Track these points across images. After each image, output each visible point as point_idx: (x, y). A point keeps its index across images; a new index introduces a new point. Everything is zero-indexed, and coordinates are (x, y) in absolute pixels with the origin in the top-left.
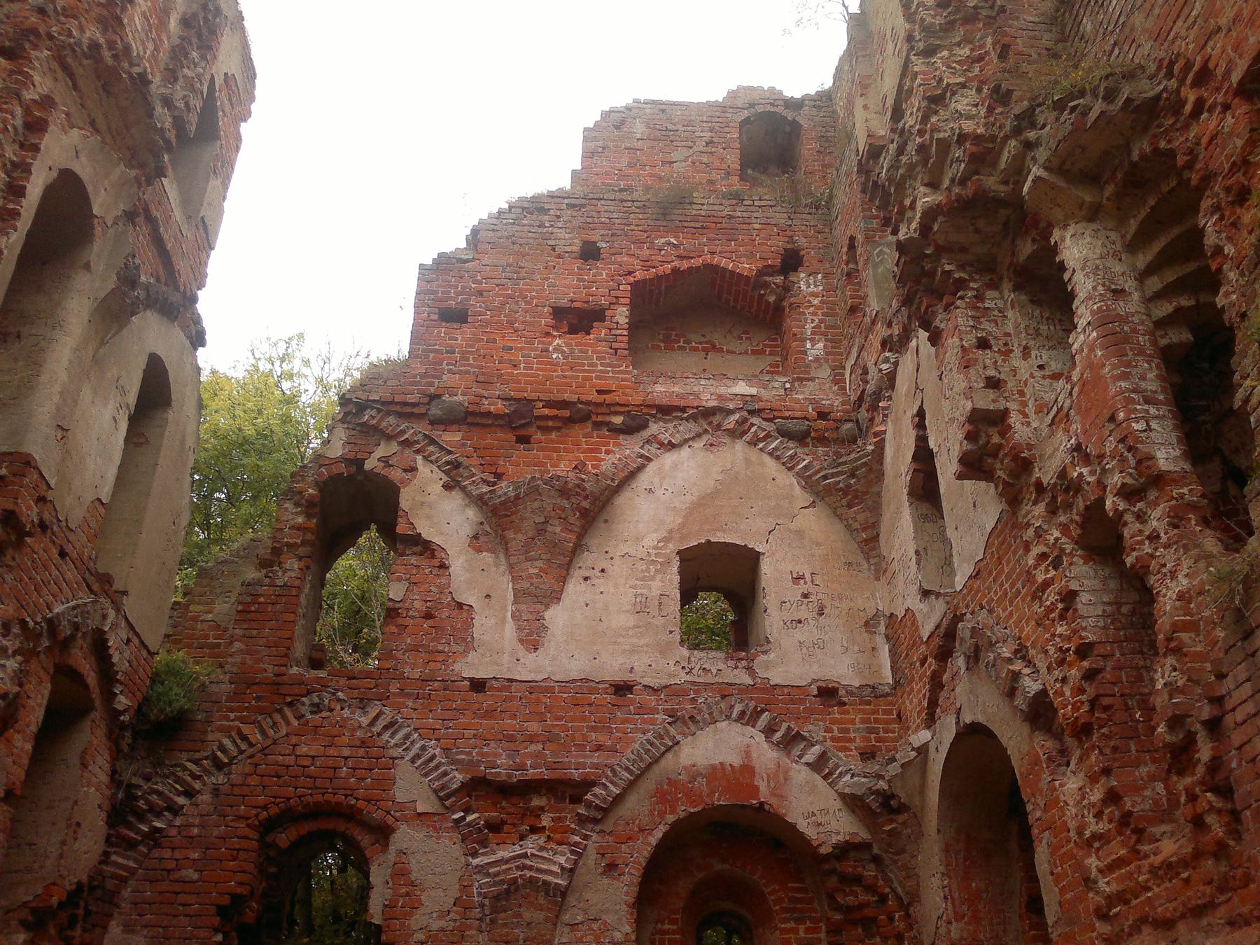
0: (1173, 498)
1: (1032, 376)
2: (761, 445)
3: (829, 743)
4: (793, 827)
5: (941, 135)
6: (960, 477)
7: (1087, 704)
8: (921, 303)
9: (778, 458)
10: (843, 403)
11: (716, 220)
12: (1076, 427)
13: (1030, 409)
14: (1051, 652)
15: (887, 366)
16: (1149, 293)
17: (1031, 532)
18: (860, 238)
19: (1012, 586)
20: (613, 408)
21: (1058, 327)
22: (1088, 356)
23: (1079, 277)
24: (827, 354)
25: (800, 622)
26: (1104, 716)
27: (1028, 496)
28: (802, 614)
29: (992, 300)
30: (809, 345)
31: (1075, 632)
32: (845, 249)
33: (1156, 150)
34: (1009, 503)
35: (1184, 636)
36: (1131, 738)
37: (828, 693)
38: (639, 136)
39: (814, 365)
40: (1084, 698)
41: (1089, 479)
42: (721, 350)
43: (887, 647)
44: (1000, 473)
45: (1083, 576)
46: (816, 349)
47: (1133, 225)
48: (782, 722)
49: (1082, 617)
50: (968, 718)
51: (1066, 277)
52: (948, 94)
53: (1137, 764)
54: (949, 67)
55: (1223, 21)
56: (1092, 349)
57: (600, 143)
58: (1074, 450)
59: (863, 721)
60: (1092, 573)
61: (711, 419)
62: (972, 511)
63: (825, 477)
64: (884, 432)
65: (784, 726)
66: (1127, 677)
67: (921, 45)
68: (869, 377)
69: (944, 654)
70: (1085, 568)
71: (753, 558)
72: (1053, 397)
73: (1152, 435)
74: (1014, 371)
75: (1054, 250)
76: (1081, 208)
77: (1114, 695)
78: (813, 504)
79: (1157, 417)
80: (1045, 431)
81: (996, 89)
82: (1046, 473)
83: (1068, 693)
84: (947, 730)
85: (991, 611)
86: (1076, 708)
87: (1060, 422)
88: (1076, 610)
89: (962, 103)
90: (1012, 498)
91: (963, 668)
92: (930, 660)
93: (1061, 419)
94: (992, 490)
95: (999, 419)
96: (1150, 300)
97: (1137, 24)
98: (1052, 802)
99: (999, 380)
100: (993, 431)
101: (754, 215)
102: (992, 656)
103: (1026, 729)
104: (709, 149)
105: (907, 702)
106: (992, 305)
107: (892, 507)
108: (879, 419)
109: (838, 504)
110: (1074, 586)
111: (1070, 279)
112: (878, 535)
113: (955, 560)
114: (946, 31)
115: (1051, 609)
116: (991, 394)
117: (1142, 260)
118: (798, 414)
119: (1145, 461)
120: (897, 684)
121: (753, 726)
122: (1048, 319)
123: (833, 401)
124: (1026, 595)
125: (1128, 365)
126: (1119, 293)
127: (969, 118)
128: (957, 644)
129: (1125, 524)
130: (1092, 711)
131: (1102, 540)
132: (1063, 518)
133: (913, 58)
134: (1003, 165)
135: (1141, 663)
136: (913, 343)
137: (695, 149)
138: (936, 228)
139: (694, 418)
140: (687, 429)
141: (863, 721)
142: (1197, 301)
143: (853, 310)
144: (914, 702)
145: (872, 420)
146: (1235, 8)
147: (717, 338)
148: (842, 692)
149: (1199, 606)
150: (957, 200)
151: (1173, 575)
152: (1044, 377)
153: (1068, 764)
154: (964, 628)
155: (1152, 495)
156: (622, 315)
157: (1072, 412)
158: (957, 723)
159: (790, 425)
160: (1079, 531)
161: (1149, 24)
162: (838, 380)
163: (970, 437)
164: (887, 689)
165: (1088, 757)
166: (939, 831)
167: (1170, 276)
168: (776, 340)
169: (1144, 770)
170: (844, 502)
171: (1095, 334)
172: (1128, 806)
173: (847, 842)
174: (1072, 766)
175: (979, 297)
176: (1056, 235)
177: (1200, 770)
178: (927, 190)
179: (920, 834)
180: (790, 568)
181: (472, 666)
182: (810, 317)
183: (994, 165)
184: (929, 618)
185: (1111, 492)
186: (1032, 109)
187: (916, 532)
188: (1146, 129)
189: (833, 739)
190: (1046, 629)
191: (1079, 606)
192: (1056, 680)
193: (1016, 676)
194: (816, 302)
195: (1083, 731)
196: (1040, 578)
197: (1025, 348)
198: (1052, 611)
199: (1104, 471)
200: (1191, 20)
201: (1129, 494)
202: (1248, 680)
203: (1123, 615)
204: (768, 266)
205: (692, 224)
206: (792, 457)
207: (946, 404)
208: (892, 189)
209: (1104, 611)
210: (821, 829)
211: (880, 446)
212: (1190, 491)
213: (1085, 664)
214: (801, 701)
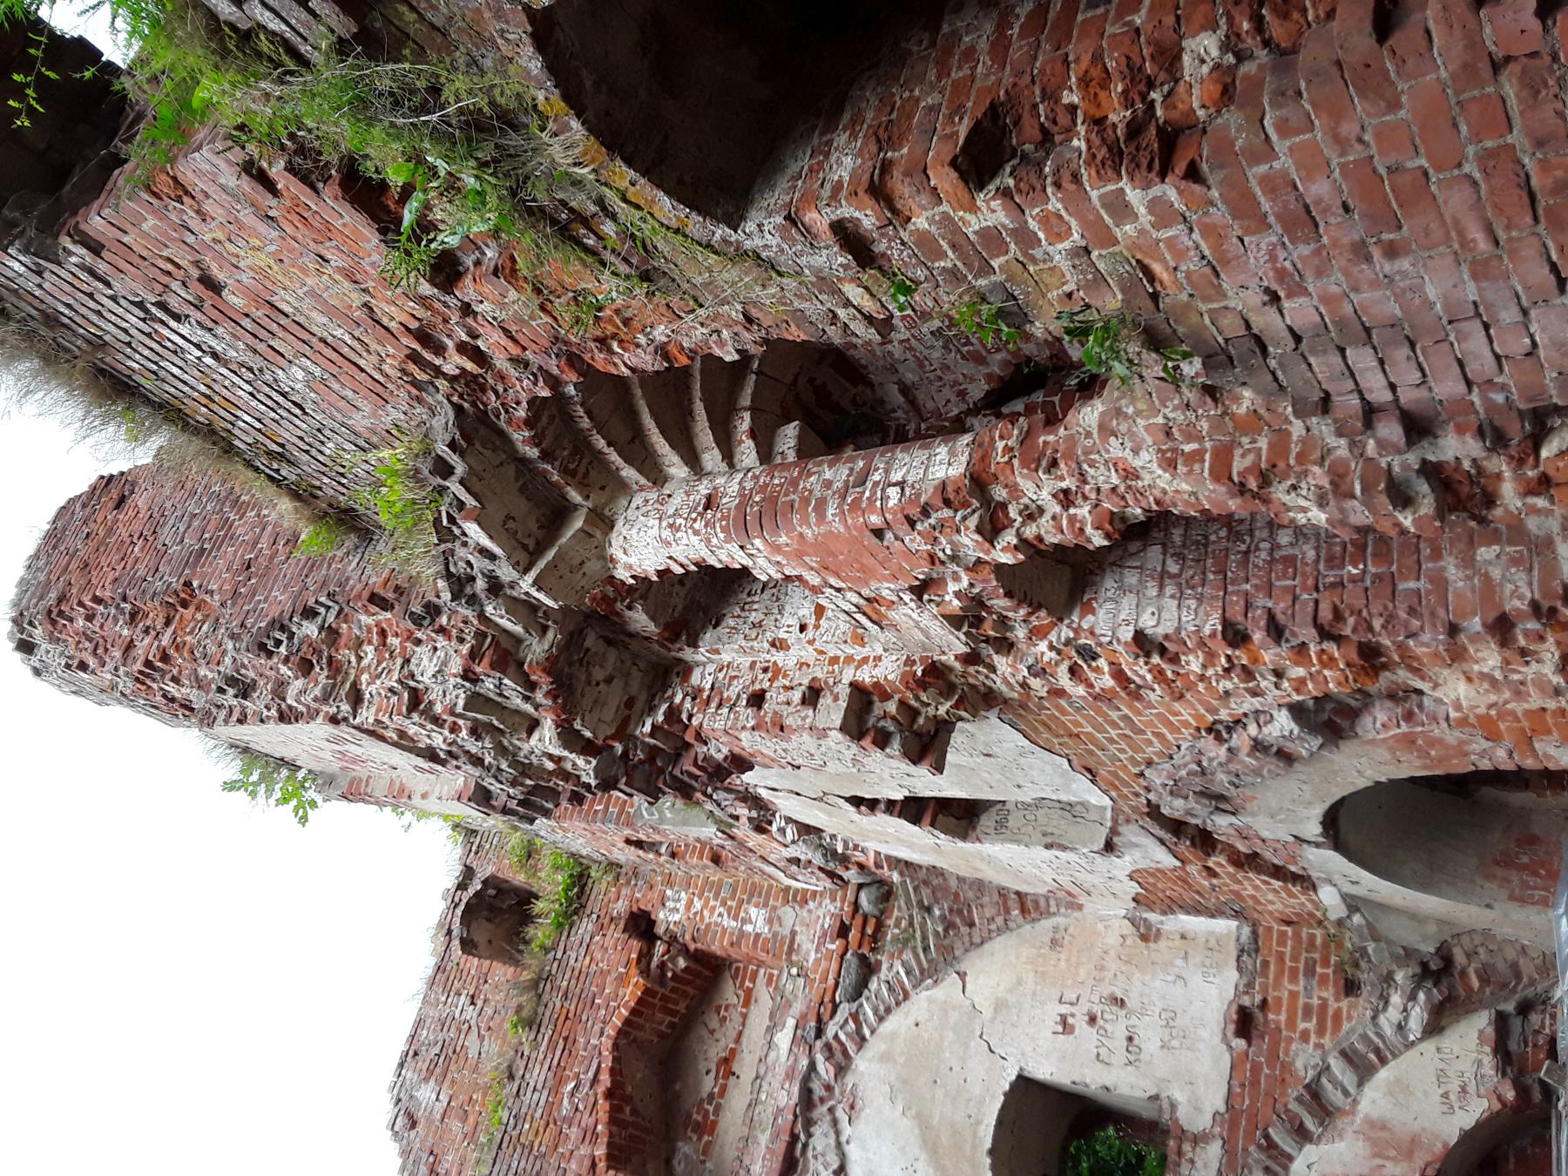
0: (1009, 462)
1: (811, 642)
2: (866, 1032)
3: (1327, 1041)
4: (1467, 1137)
5: (461, 702)
6: (939, 768)
7: (1325, 645)
8: (690, 775)
9: (888, 1010)
10: (833, 900)
11: (562, 1018)
12: (886, 590)
13: (858, 652)
14: (1229, 685)
15: (789, 831)
16: (723, 467)
17: (1035, 683)
18: (627, 832)
19: (1114, 725)
21: (756, 598)
22: (785, 554)
23: (678, 552)
24: (766, 905)
25: (1130, 1039)
26: (1351, 621)
27: (981, 678)
28: (1120, 1032)
29: (702, 678)
31: (1202, 643)
32: (641, 852)
33: (528, 423)
34: (989, 707)
35: (1238, 465)
36: (1394, 585)
37: (1245, 1023)
38: (434, 1097)
39: (776, 927)
40: (1313, 649)
41: (965, 583)
42: (733, 1051)
43: (1183, 917)
44: (942, 711)
45: (1116, 615)
47: (629, 473)
48: (1287, 1111)
49: (1178, 630)
50: (1313, 829)
51: (679, 570)
52: (412, 684)
53: (1440, 583)
54: (379, 676)
55: (357, 299)
56: (777, 549)
57: (425, 1156)
58: (920, 599)
59: (1294, 978)
60: (1109, 605)
61: (816, 1098)
62: (983, 757)
63: (926, 949)
64: (878, 853)
65: (1293, 1106)
66: (1285, 577)
67: (346, 708)
68: (803, 857)
69: (1205, 841)
70: (1101, 613)
71: (1025, 1089)
72: (843, 616)
73: (910, 479)
74: (802, 665)
75: (643, 581)
76: (590, 536)
77: (1317, 602)
78: (962, 976)
79: (887, 471)
80: (889, 635)
81: (417, 621)
82: (951, 646)
83: (1300, 672)
84: (1325, 861)
85: (1149, 763)
86: (1329, 662)
87: (878, 612)
88: (1166, 637)
89: (425, 665)
90: (984, 700)
91: (1233, 819)
92: (1210, 864)
93: (873, 608)
94: (967, 726)
95: (863, 697)
96: (731, 465)
97: (366, 422)
98: (1488, 727)
99: (810, 688)
100: (878, 708)
101: (572, 962)
102: (1222, 777)
103: (1348, 747)
104: (480, 1003)
105: (1270, 908)
106: (710, 679)
107: (979, 864)
108: (858, 856)
109: (966, 939)
110: (1127, 634)
111: (682, 566)
112: (1018, 893)
113: (1064, 798)
114: (338, 671)
115: (1159, 674)
116: (825, 701)
117: (676, 468)
118: (834, 966)
119: (946, 496)
120: (1237, 915)
121: (1290, 1159)
122: (743, 609)
123: (826, 912)
124: (1131, 707)
125: (806, 501)
126: (709, 503)
127: (445, 663)
128: (1193, 821)
129: (1040, 539)
130: (1338, 639)
131: (1060, 578)
132: (1020, 633)
133: (358, 720)
134: (518, 629)
135: (1264, 555)
136: (764, 793)
137: (473, 1022)
138: (588, 734)
139: (809, 1123)
140: (821, 1139)
141: (1294, 978)
142: (745, 409)
143: (716, 859)
144: (1273, 898)
145: (861, 866)
146: (337, 277)
147: (715, 1052)
148: (1246, 1001)
149: (1189, 438)
150: (555, 698)
151: (1130, 474)
152: (817, 627)
153: (1420, 692)
154: (1174, 807)
155: (999, 493)
157: (866, 592)
158: (1318, 845)
159: (848, 980)
160: (1043, 613)
161: (367, 408)
162: (802, 898)
163: (882, 741)
164: (1246, 931)
165: (1417, 658)
166: (1488, 906)
167: (704, 436)
168: (738, 969)
169: (1452, 570)
170: (964, 930)
171: (758, 542)
172: (1522, 605)
173: (1496, 1052)
174: (1424, 686)
175: (696, 694)
176: (622, 574)
177: (1499, 464)
178: (536, 736)
179: (1486, 934)
180: (1048, 1034)
183: (518, 641)
184: (1149, 852)
185: (987, 553)
186: (449, 575)
187: (1018, 842)
188: (502, 434)
189: (1321, 1031)
190: (1190, 686)
191: (1161, 631)
192: (1277, 686)
193: (1259, 746)
195: (1371, 658)
196: (1108, 682)
197: (773, 644)
198: (1161, 672)
199: (954, 558)
200: (355, 344)
201: (991, 529)
202: (1342, 351)
203: (1181, 570)
204: (639, 961)
205: (558, 1053)
206: (890, 989)
207: (832, 767)
208: (529, 782)
209: (1172, 597)
210: (1472, 1088)
211: (895, 863)
212: (1002, 438)
213: (1258, 636)
214: (1256, 1069)
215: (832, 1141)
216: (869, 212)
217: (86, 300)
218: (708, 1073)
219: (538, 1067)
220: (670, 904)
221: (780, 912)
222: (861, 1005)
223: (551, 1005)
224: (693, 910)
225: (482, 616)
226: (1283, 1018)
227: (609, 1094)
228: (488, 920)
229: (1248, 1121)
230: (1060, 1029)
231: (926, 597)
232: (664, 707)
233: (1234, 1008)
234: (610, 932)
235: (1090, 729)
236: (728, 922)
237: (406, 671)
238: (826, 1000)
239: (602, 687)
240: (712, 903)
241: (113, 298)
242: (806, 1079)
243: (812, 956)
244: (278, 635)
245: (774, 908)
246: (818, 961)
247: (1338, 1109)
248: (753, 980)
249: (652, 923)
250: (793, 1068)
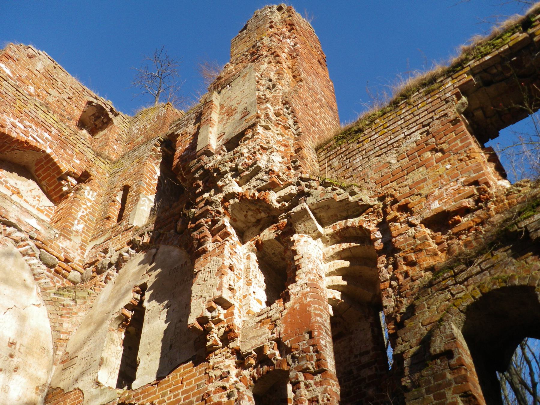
2: (27, 258)
10: (80, 261)
24: (83, 232)
30: (76, 222)
38: (38, 69)
44: (215, 335)
46: (79, 227)
76: (314, 231)
78: (39, 305)
101: (79, 145)
104: (68, 100)
111: (298, 260)
118: (55, 253)
162: (83, 248)
182: (83, 209)
194: (89, 204)
216: (455, 362)
217: (433, 108)
219: (44, 117)
220: (91, 192)
221: (80, 237)
224: (87, 201)
225: (291, 184)
228: (93, 115)
230: (11, 341)
231: (274, 342)
235: (184, 388)
236: (80, 214)
237: (275, 150)
239: (245, 213)
240: (88, 210)
241: (432, 118)
242: (15, 226)
243: (61, 245)
244: (290, 110)
245: (81, 235)
246: (59, 247)
248: (46, 215)
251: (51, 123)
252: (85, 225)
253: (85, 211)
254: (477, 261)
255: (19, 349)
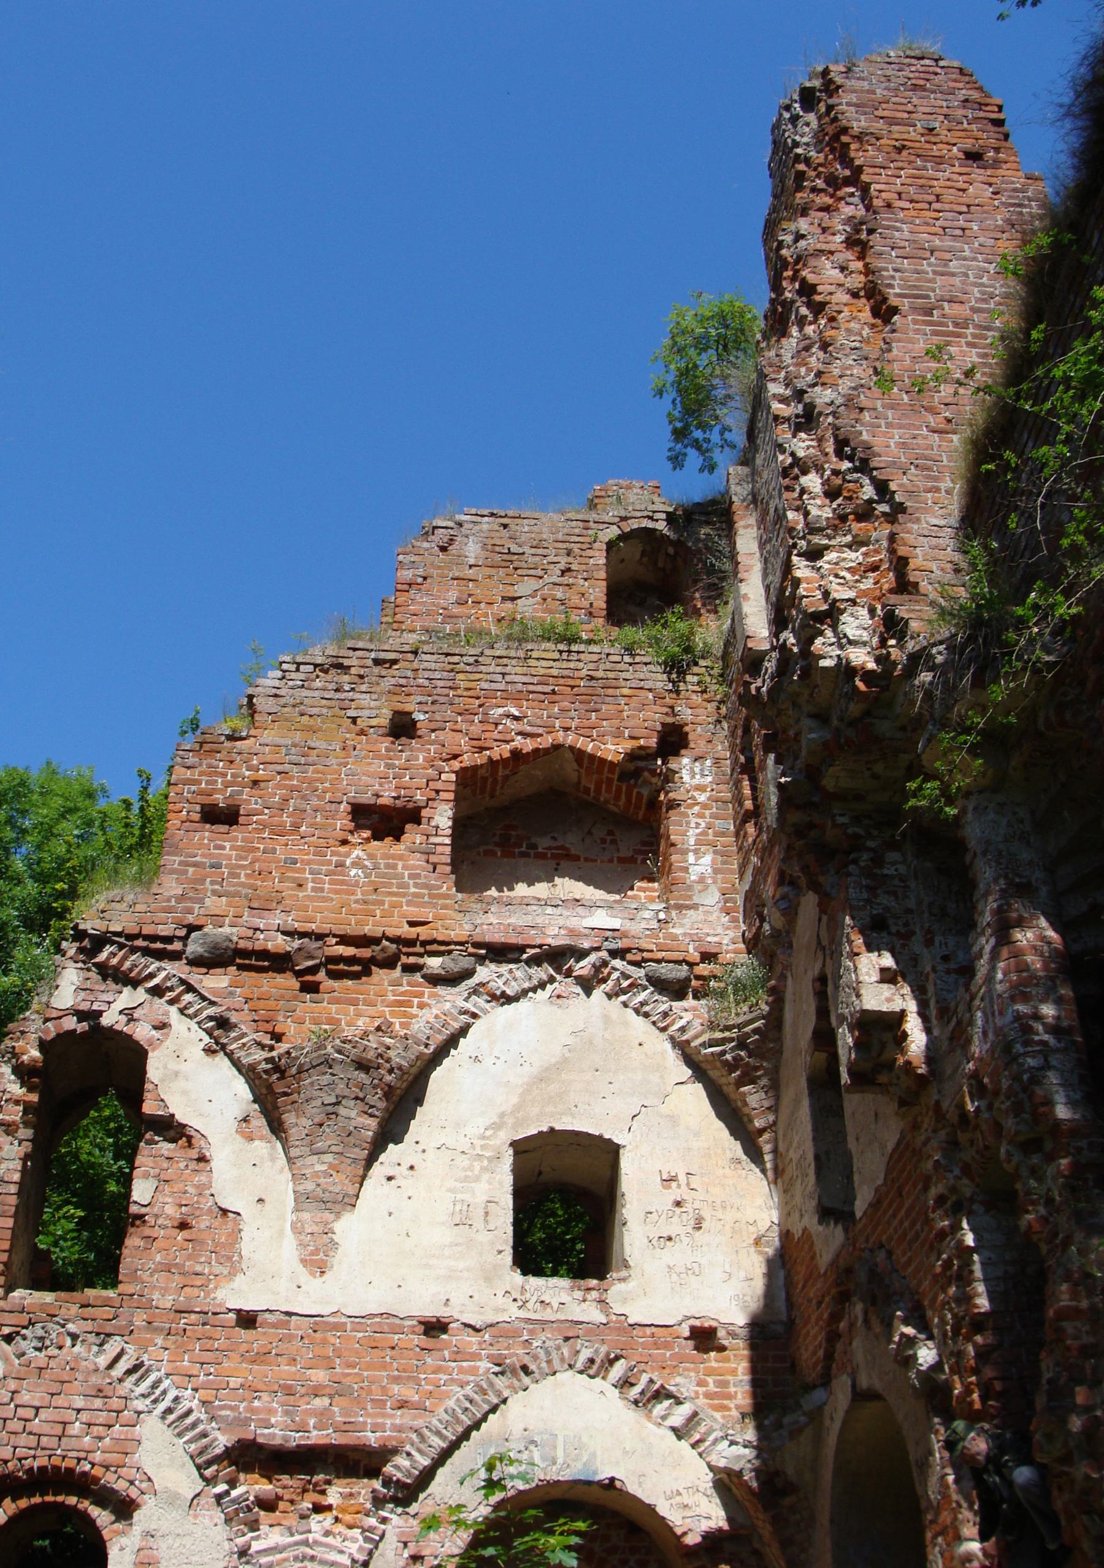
3: (702, 1401)
9: (646, 1015)
11: (571, 682)
20: (432, 946)
24: (716, 871)
25: (670, 1239)
38: (472, 561)
57: (421, 572)
101: (624, 675)
104: (565, 580)
139: (535, 961)
148: (721, 1333)
152: (948, 972)
156: (442, 817)
175: (878, 861)
181: (238, 1294)
182: (693, 821)
197: (929, 931)
205: (539, 688)
214: (667, 1346)
215: (527, 985)
218: (554, 838)
222: (645, 988)
223: (581, 665)
226: (714, 1364)
227: (516, 754)
228: (643, 554)
229: (625, 1342)
232: (860, 831)
233: (714, 1324)
234: (657, 708)
238: (645, 954)
240: (707, 813)
247: (650, 1411)
249: (676, 753)
250: (579, 935)
251: (542, 671)
252: (715, 852)
253: (700, 821)
254: (565, 1524)
255: (688, 1184)
